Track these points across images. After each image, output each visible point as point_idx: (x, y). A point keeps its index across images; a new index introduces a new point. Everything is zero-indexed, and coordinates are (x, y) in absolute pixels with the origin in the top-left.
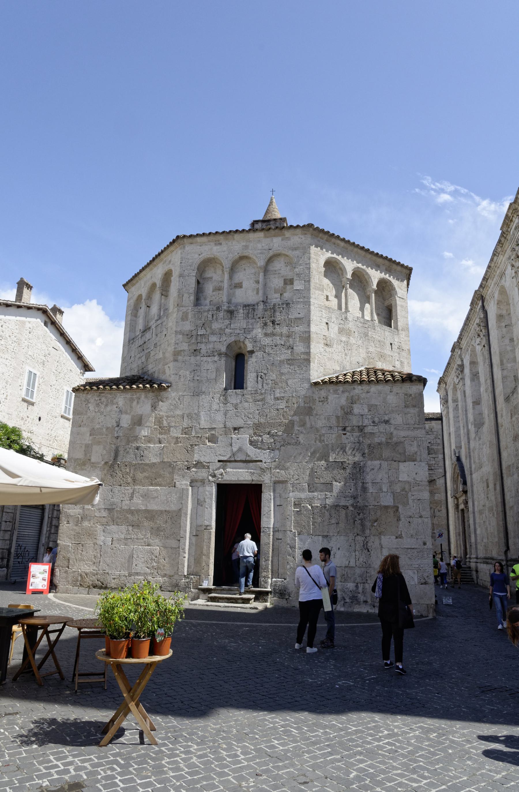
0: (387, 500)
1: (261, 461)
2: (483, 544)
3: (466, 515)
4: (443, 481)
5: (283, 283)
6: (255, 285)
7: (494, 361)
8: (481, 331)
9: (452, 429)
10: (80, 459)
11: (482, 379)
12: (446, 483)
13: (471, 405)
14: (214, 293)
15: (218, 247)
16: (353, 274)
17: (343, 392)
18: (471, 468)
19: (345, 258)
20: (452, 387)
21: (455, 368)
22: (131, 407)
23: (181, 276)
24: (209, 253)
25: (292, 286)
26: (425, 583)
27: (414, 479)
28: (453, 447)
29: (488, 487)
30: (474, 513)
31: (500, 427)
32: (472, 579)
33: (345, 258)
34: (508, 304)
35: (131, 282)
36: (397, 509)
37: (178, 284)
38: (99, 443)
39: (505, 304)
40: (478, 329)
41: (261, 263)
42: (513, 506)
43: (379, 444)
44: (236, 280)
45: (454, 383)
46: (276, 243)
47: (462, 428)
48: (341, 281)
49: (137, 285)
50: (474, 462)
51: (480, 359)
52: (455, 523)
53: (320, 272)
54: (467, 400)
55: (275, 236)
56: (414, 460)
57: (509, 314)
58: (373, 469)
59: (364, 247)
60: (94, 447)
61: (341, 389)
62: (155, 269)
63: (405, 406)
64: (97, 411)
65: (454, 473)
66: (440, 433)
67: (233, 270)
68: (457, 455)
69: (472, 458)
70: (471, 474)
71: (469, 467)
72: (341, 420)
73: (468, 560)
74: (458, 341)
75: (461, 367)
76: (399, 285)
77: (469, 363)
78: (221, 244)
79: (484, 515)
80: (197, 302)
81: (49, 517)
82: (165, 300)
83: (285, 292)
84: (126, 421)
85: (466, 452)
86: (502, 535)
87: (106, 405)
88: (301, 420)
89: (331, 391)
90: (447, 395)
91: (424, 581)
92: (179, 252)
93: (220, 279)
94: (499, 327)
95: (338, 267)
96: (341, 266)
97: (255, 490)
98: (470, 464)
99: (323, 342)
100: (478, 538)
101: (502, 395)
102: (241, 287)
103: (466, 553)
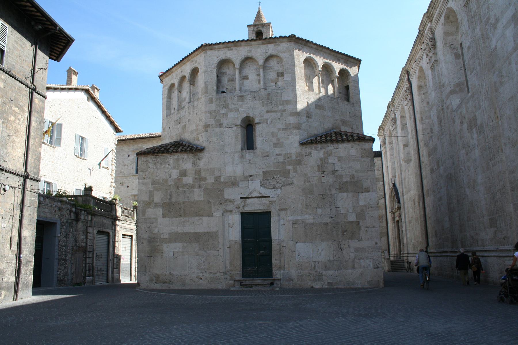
0: (352, 218)
6: (257, 78)
7: (417, 117)
9: (389, 164)
11: (409, 129)
12: (385, 203)
13: (402, 148)
15: (230, 52)
17: (321, 148)
18: (403, 191)
19: (318, 57)
20: (388, 133)
22: (178, 164)
23: (206, 72)
26: (378, 267)
27: (369, 203)
28: (390, 176)
29: (415, 204)
30: (405, 222)
31: (422, 163)
34: (425, 78)
37: (204, 78)
38: (158, 190)
40: (406, 94)
41: (261, 62)
46: (271, 49)
47: (396, 163)
50: (406, 187)
51: (407, 115)
55: (269, 43)
56: (368, 192)
57: (426, 85)
60: (155, 192)
66: (381, 166)
67: (241, 68)
70: (403, 196)
74: (391, 101)
75: (394, 120)
76: (352, 71)
78: (232, 49)
82: (193, 87)
83: (278, 82)
84: (175, 174)
85: (399, 180)
86: (424, 237)
90: (385, 139)
92: (203, 55)
94: (419, 94)
95: (312, 63)
97: (266, 216)
102: (248, 79)
103: (400, 251)
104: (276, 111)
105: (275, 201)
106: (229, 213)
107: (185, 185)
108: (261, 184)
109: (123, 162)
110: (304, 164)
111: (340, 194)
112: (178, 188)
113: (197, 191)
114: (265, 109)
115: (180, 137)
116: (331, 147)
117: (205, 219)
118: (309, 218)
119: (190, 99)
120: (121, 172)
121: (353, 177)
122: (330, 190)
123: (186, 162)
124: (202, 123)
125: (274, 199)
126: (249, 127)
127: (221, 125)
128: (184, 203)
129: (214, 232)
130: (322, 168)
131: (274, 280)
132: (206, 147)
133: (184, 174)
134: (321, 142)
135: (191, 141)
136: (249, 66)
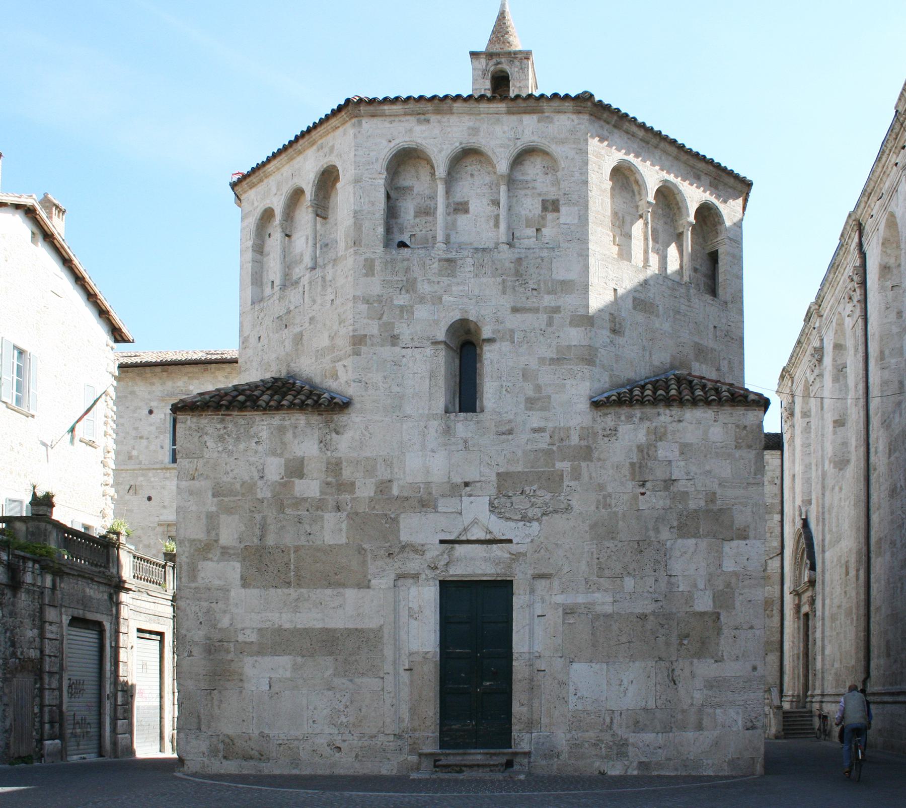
0: (704, 603)
1: (510, 541)
2: (833, 672)
3: (810, 623)
4: (778, 564)
5: (540, 208)
6: (490, 210)
7: (870, 350)
8: (854, 291)
10: (200, 541)
14: (418, 220)
16: (659, 191)
17: (641, 419)
18: (823, 540)
20: (801, 387)
21: (808, 353)
22: (283, 443)
23: (357, 181)
24: (407, 139)
25: (556, 214)
28: (798, 502)
29: (847, 574)
30: (823, 619)
31: (872, 471)
32: (813, 729)
33: (648, 163)
35: (248, 180)
36: (718, 616)
37: (352, 200)
38: (229, 511)
39: (894, 245)
40: (851, 285)
41: (503, 167)
42: (880, 607)
43: (696, 511)
44: (458, 197)
45: (807, 380)
48: (637, 207)
49: (261, 188)
50: (830, 531)
51: (850, 343)
52: (794, 637)
53: (604, 191)
54: (825, 416)
56: (745, 538)
57: (899, 265)
58: (685, 553)
59: (675, 141)
60: (223, 517)
61: (638, 415)
62: (299, 159)
63: (736, 447)
64: (220, 449)
65: (797, 549)
68: (804, 517)
69: (827, 523)
70: (823, 551)
71: (820, 538)
72: (637, 469)
73: (808, 699)
74: (816, 303)
75: (819, 352)
76: (729, 210)
77: (832, 346)
78: (428, 121)
79: (838, 622)
80: (394, 240)
81: (111, 647)
82: (323, 225)
83: (544, 226)
84: (274, 469)
85: (818, 512)
86: (861, 655)
87: (238, 439)
88: (573, 469)
89: (623, 418)
90: (793, 402)
91: (751, 724)
93: (427, 192)
94: (882, 288)
95: (632, 179)
96: (638, 177)
97: (502, 589)
98: (823, 535)
99: (608, 325)
100: (827, 663)
101: (879, 414)
102: (466, 211)
103: (806, 688)
104: (536, 310)
105: (525, 555)
106: (411, 581)
107: (299, 502)
108: (493, 508)
109: (136, 429)
110: (599, 459)
111: (679, 541)
112: (281, 508)
113: (330, 518)
114: (506, 302)
115: (288, 365)
116: (665, 417)
117: (351, 594)
118: (603, 601)
119: (315, 259)
120: (130, 458)
121: (711, 497)
122: (657, 530)
123: (303, 436)
124: (345, 331)
125: (522, 549)
126: (465, 347)
127: (394, 339)
128: (297, 549)
129: (372, 630)
130: (640, 470)
131: (516, 754)
132: (357, 405)
133: (296, 469)
134: (642, 402)
135: (317, 380)
136: (472, 175)
